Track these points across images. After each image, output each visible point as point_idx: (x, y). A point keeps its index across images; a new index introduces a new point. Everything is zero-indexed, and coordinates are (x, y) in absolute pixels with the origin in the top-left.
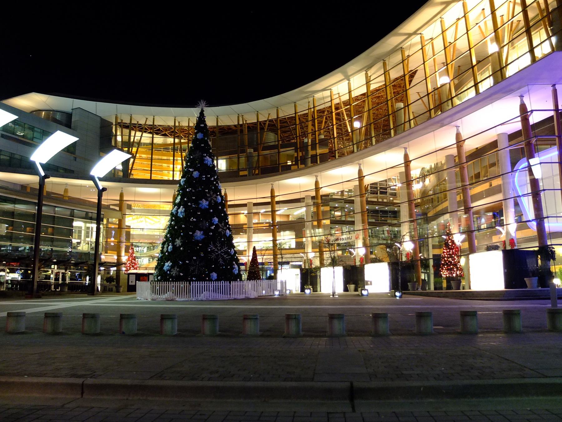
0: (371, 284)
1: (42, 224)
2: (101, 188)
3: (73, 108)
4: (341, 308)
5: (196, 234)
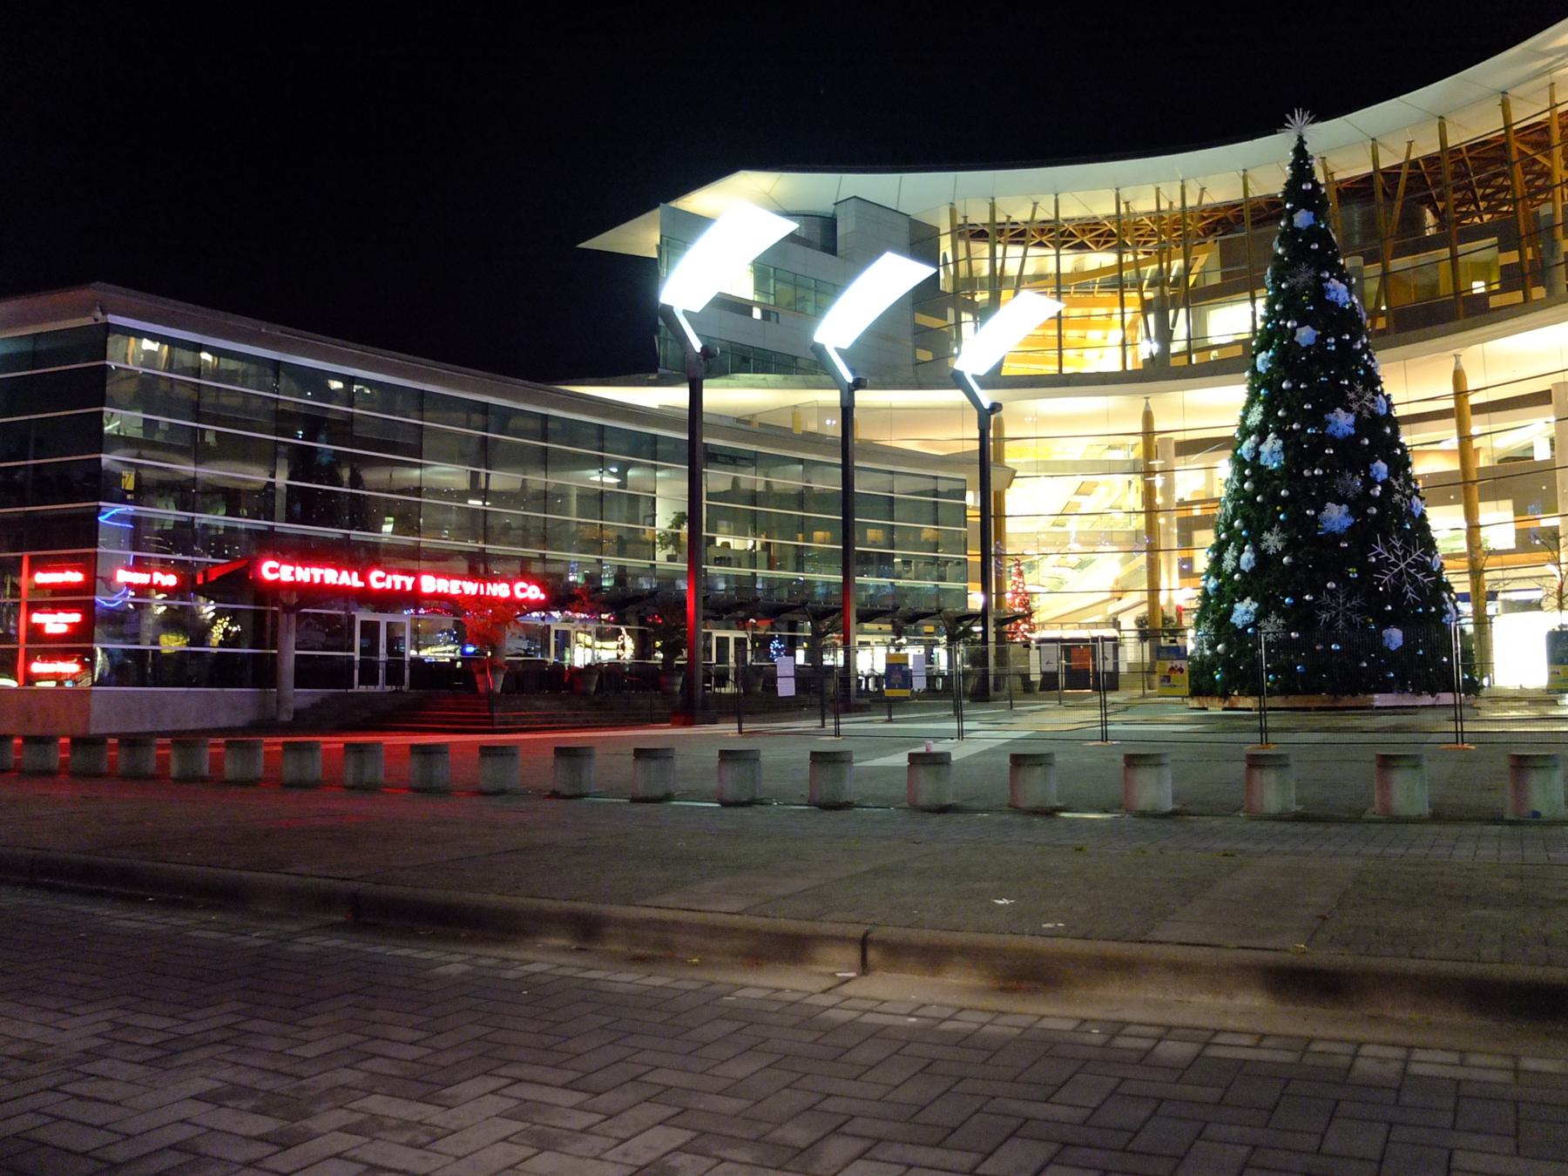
1: (856, 519)
2: (987, 405)
5: (1325, 513)
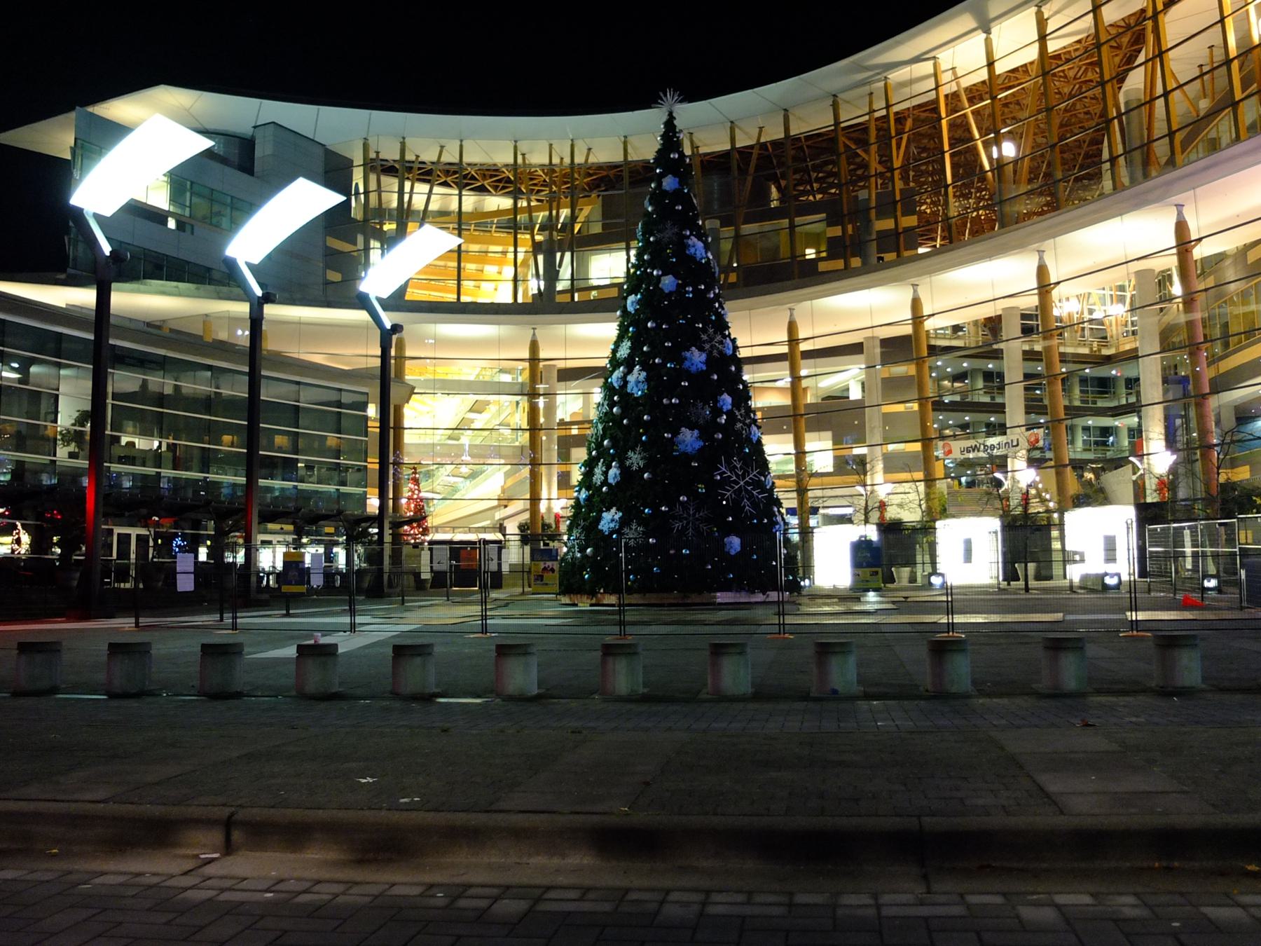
0: (1082, 561)
2: (388, 326)
3: (258, 124)
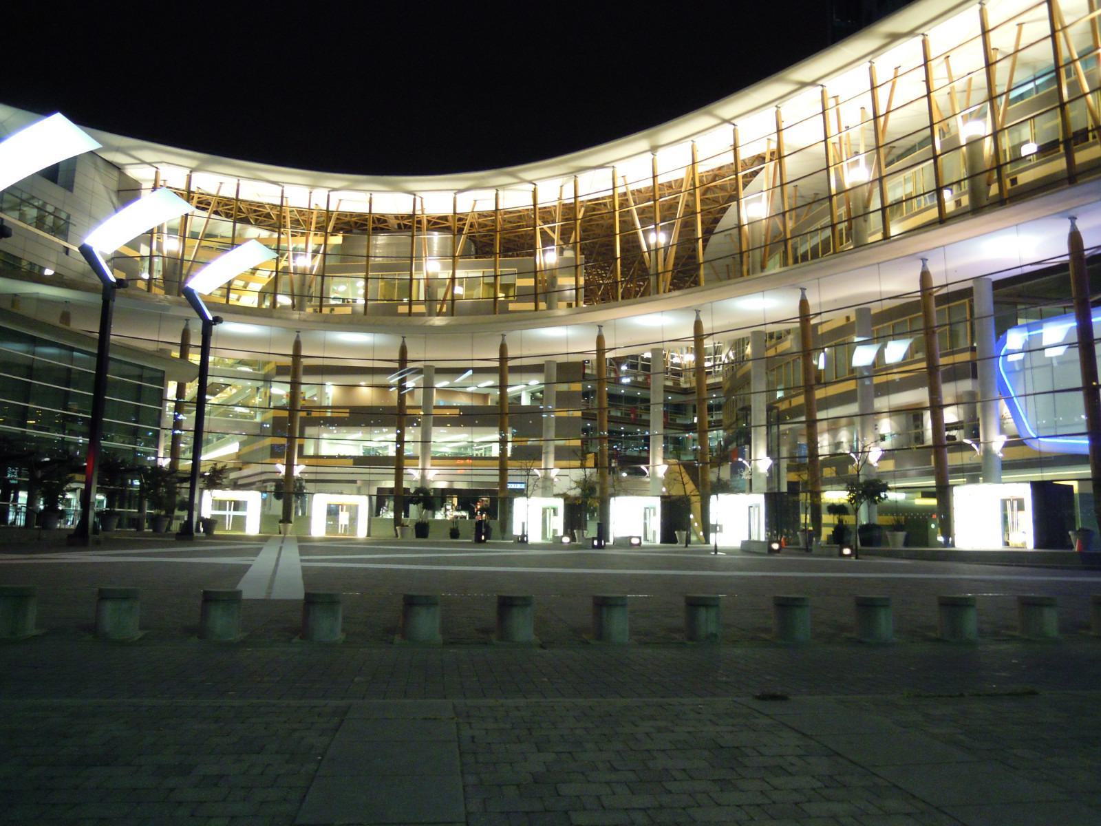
4: (164, 557)
